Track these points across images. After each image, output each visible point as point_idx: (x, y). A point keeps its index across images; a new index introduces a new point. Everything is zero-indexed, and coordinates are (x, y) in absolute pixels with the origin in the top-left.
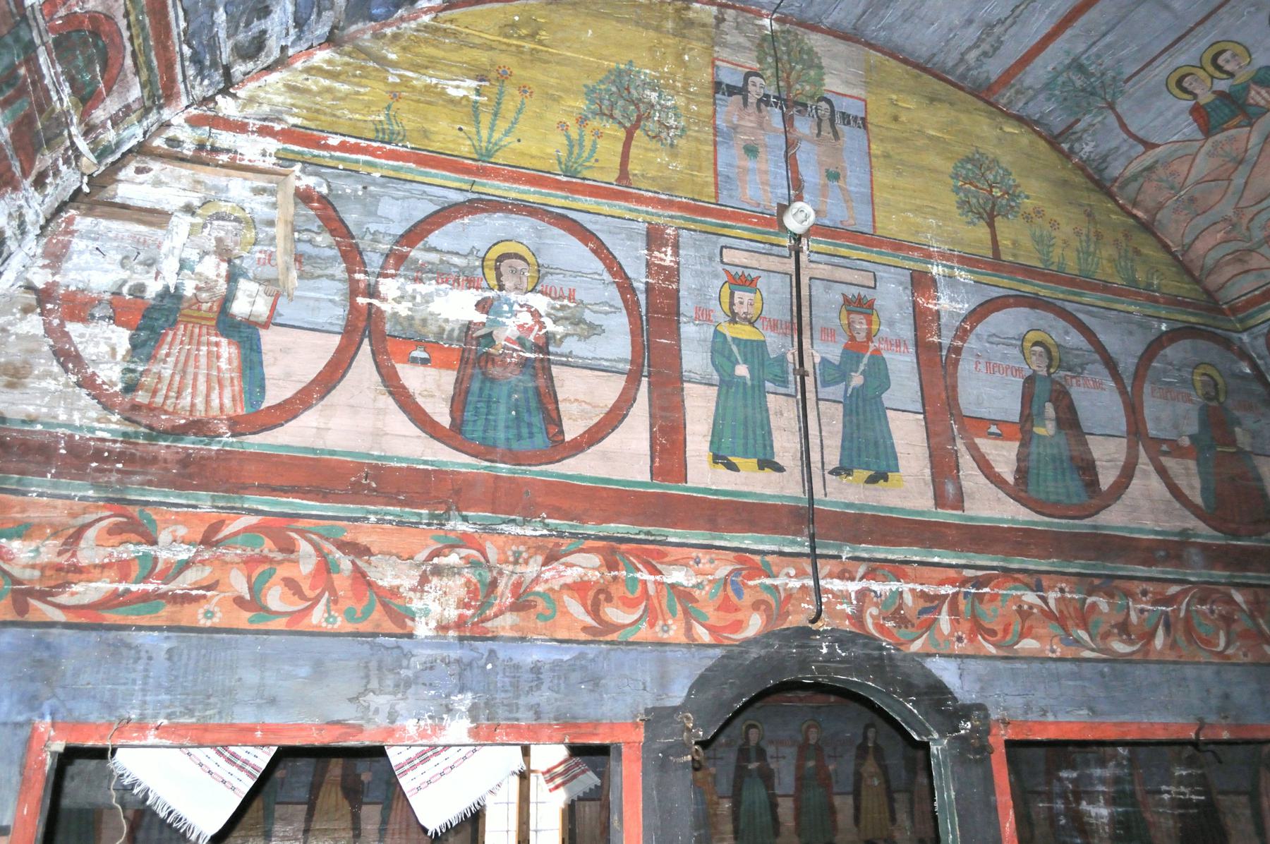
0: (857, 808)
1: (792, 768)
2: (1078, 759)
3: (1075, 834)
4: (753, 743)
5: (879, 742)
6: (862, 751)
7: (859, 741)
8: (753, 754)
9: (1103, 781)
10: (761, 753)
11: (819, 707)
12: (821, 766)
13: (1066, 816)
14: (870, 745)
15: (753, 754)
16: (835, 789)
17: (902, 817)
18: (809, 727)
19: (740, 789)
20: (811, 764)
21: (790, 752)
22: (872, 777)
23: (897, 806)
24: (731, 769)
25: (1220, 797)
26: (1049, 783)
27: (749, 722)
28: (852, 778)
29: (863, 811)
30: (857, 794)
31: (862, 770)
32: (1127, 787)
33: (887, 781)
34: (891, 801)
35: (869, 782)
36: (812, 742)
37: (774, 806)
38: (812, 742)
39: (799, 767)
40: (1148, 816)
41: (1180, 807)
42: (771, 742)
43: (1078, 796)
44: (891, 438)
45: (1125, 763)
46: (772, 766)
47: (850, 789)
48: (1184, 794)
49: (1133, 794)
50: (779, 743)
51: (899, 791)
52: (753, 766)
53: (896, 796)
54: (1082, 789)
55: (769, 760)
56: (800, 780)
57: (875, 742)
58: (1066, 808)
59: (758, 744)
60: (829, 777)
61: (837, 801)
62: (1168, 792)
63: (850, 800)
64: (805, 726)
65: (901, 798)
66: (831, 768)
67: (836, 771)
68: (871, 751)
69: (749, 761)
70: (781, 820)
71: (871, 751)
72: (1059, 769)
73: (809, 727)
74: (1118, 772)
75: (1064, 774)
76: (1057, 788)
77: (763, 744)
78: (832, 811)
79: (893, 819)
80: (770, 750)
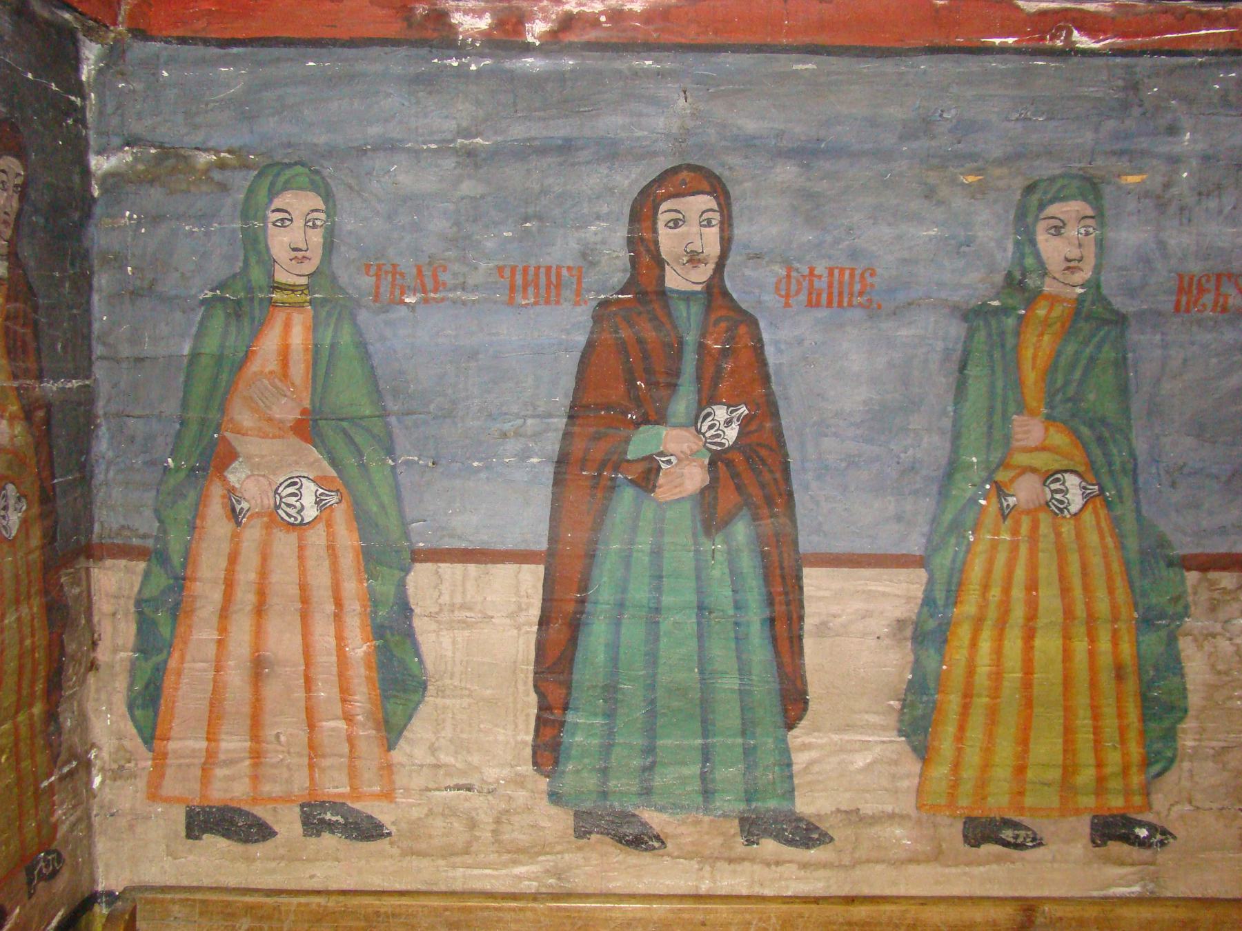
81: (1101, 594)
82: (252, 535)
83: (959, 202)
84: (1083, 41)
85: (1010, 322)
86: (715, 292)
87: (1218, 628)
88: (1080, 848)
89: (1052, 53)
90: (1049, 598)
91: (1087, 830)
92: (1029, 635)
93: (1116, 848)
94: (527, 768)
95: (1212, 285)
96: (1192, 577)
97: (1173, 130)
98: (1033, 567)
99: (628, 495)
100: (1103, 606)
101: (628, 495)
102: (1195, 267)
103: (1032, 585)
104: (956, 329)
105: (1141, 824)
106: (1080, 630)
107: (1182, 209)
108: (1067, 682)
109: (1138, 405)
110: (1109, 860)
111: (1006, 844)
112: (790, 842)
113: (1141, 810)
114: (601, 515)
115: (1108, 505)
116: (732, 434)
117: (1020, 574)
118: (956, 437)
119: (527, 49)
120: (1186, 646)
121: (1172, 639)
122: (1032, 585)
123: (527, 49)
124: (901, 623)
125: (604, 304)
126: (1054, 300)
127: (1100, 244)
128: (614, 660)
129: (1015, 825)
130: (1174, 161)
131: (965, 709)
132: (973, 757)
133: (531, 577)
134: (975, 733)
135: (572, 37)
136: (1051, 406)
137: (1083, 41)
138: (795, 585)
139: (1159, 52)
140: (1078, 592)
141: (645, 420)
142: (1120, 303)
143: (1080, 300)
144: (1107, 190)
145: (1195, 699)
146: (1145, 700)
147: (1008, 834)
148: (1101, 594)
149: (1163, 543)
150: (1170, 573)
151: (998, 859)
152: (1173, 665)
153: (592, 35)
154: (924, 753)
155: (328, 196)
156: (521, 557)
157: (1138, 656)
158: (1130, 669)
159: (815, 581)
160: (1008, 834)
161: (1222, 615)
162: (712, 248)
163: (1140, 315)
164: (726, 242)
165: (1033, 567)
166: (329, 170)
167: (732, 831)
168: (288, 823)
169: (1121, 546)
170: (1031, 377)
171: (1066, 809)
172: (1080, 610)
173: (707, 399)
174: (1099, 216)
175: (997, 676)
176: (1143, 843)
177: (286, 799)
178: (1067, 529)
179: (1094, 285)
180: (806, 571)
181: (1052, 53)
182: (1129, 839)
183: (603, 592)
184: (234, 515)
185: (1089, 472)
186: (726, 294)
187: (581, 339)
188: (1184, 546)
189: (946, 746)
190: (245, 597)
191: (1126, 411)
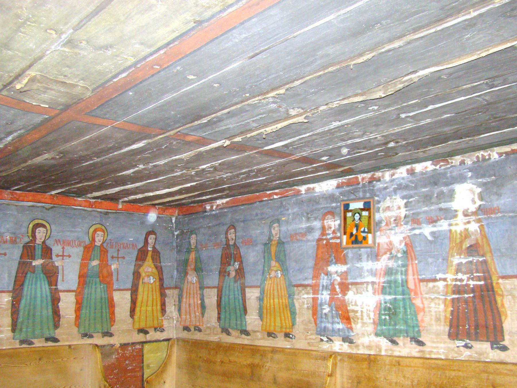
0: (134, 302)
1: (77, 267)
2: (350, 255)
3: (338, 320)
4: (39, 241)
5: (158, 247)
6: (142, 255)
7: (140, 245)
8: (38, 252)
9: (373, 273)
10: (47, 252)
11: (106, 213)
12: (104, 264)
13: (330, 305)
14: (150, 249)
15: (38, 252)
16: (115, 286)
17: (171, 309)
18: (95, 231)
19: (22, 285)
20: (95, 263)
21: (77, 252)
22: (148, 276)
23: (167, 300)
24: (15, 266)
25: (500, 281)
26: (316, 276)
27: (36, 222)
28: (131, 277)
29: (138, 304)
30: (134, 291)
31: (141, 270)
32: (399, 277)
33: (161, 280)
34: (163, 295)
35: (146, 280)
36: (98, 243)
37: (55, 300)
38: (98, 243)
39: (83, 266)
40: (418, 302)
41: (454, 293)
42: (57, 241)
43: (345, 287)
44: (59, 312)
45: (399, 255)
46: (57, 264)
47: (129, 285)
48: (461, 280)
49: (405, 282)
50: (66, 243)
51: (170, 288)
52: (37, 263)
53: (167, 292)
54: (350, 281)
55: (54, 257)
56: (83, 278)
57: (154, 248)
58: (332, 299)
59: (44, 242)
60: (111, 274)
61: (117, 296)
62: (445, 280)
63: (128, 295)
64: (91, 230)
65: (172, 295)
66: (113, 267)
67: (117, 270)
68: (150, 254)
69: (33, 258)
70: (62, 313)
71: (150, 254)
72: (328, 263)
73: (95, 231)
74: (391, 264)
75: (333, 268)
76: (324, 280)
77: (49, 243)
78: (111, 305)
79: (163, 310)
80: (56, 249)
81: (283, 292)
82: (189, 285)
83: (262, 225)
84: (275, 197)
85: (270, 245)
86: (235, 243)
87: (299, 298)
88: (283, 338)
89: (271, 200)
90: (276, 293)
91: (284, 335)
92: (274, 299)
93: (288, 339)
94: (217, 321)
95: (295, 235)
96: (295, 288)
97: (288, 210)
98: (274, 287)
99: (227, 277)
100: (283, 294)
101: (227, 277)
102: (293, 233)
103: (273, 290)
104: (263, 247)
105: (291, 334)
106: (280, 299)
107: (133, 245)
108: (279, 308)
109: (287, 258)
110: (286, 341)
111: (273, 337)
112: (246, 335)
113: (291, 332)
114: (224, 280)
115: (284, 276)
116: (238, 266)
117: (272, 288)
118: (264, 266)
119: (213, 210)
120: (295, 301)
121: (293, 300)
122: (273, 290)
123: (213, 210)
124: (257, 297)
125: (223, 247)
126: (275, 240)
127: (280, 230)
128: (225, 304)
129: (274, 334)
130: (289, 215)
131: (267, 312)
132: (268, 321)
133: (216, 290)
134: (268, 317)
135: (218, 208)
136: (276, 259)
137: (275, 197)
138: (244, 290)
139: (285, 197)
140: (280, 291)
141: (228, 265)
142: (283, 240)
143: (278, 240)
144: (281, 221)
145: (297, 312)
146: (290, 311)
147: (273, 335)
148: (283, 292)
149: (292, 282)
150: (292, 288)
151: (272, 339)
152: (293, 303)
153: (220, 207)
154: (262, 320)
155: (196, 235)
156: (214, 287)
157: (289, 302)
158: (106, 299)
159: (247, 290)
160: (273, 335)
161: (300, 295)
162: (234, 238)
163: (286, 242)
164: (235, 236)
165: (274, 287)
166: (196, 231)
167: (129, 322)
168: (192, 329)
169: (286, 283)
170: (273, 254)
171: (281, 331)
172: (280, 295)
173: (235, 261)
174: (279, 226)
175: (270, 306)
176: (291, 338)
177: (193, 325)
178: (279, 280)
179: (279, 238)
180: (246, 289)
181: (271, 200)
182: (289, 337)
183: (224, 293)
184: (188, 282)
185: (282, 271)
186: (236, 245)
187: (221, 253)
188: (294, 283)
189: (265, 320)
190: (272, 297)
191: (286, 259)
